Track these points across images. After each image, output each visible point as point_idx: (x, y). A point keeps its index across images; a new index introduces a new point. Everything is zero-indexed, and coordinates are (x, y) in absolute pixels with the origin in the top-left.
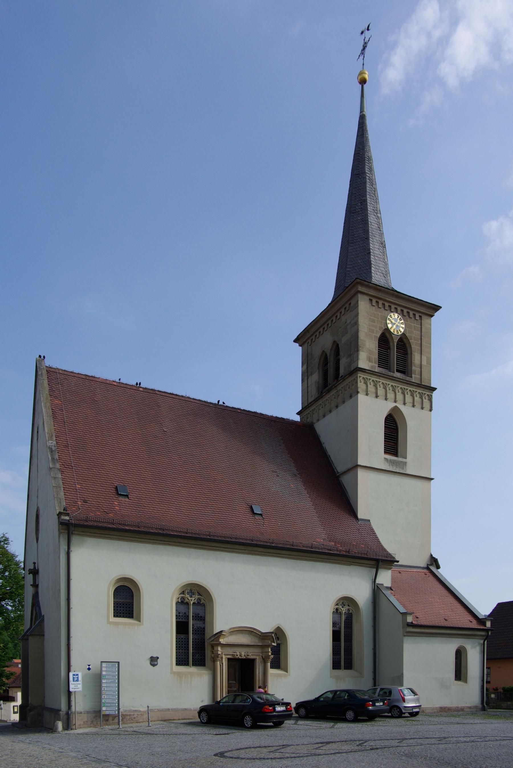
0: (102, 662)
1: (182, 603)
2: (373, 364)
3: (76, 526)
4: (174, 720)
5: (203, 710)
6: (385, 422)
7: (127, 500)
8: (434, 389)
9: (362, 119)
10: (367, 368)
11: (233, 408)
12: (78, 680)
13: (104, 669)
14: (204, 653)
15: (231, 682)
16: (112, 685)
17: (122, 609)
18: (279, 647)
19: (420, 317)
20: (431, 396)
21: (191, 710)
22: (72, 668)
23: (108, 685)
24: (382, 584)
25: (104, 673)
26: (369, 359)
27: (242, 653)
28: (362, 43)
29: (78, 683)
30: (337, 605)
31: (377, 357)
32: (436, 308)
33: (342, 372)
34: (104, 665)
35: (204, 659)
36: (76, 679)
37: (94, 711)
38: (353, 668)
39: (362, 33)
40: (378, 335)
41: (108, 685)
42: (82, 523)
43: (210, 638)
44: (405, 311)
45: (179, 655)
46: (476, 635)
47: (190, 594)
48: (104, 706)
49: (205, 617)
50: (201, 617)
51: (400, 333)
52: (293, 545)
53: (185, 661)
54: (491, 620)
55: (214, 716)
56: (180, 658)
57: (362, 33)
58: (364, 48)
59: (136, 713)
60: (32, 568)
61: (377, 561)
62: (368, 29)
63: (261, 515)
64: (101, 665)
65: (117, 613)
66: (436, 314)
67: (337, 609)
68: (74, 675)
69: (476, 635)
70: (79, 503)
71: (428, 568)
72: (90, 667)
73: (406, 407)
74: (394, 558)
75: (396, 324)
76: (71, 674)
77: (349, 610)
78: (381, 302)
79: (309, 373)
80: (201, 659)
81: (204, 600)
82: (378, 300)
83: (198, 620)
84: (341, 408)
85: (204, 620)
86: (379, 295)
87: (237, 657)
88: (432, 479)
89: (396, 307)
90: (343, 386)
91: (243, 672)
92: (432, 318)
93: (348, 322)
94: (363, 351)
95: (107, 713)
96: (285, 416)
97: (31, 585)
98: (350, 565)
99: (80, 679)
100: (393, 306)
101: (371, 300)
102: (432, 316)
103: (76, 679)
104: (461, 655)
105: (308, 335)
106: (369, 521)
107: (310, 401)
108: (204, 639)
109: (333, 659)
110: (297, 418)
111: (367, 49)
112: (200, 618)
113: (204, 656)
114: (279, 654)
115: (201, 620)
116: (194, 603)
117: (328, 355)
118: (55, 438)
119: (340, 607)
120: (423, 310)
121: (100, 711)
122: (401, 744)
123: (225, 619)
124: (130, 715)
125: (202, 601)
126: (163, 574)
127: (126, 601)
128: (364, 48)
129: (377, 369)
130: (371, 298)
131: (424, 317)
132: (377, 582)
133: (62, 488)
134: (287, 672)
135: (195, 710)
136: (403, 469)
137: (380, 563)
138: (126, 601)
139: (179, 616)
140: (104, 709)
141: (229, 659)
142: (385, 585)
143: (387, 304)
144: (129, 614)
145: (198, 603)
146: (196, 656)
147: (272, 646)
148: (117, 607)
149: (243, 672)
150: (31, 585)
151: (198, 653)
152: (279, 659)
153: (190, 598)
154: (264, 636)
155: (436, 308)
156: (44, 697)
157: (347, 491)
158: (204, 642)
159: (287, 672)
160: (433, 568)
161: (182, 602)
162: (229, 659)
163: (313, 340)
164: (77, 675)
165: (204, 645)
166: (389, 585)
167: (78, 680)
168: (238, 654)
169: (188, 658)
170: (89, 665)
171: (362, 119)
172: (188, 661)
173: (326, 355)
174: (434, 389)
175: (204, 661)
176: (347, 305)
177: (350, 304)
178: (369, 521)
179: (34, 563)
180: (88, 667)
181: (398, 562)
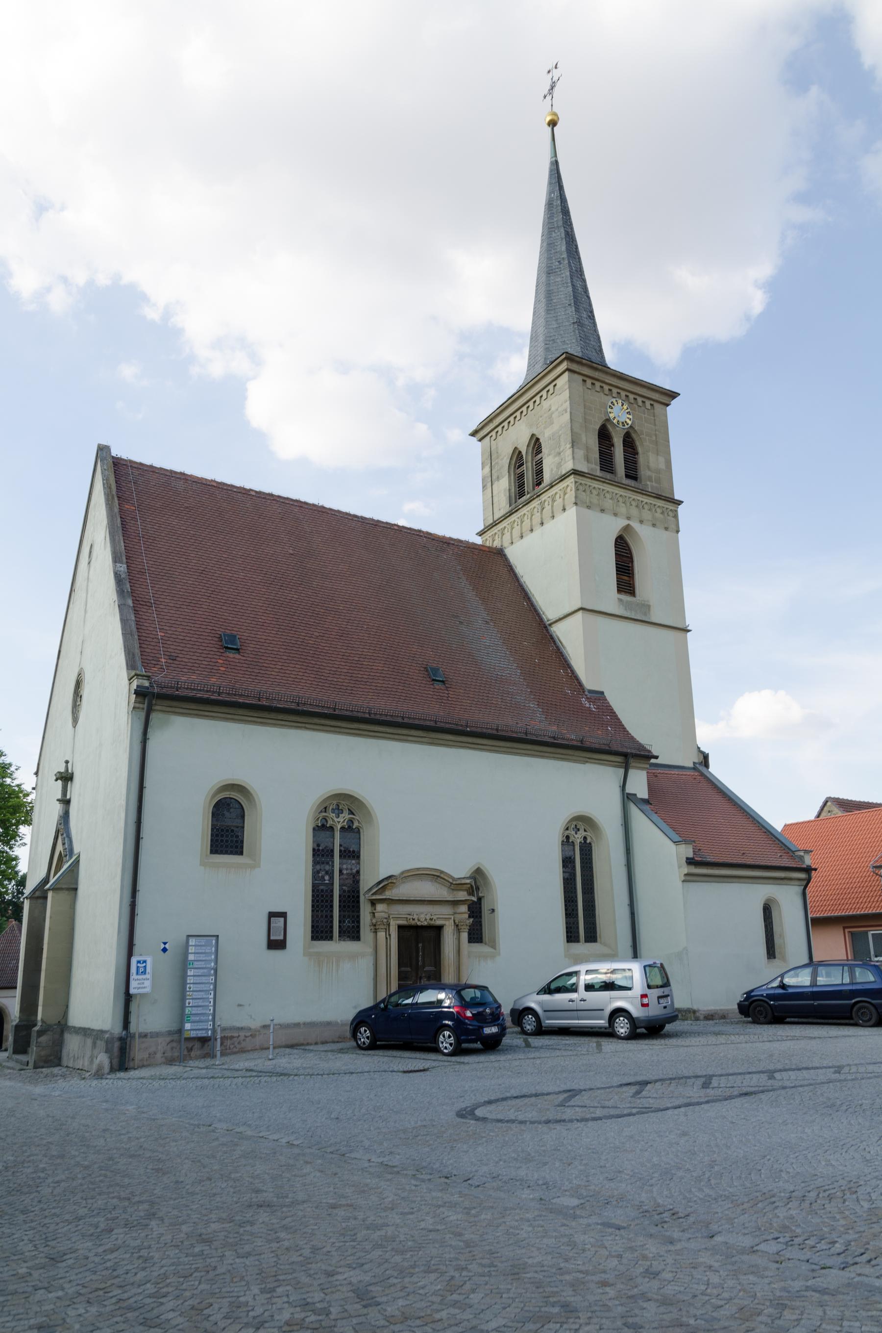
0: (189, 936)
1: (322, 828)
2: (593, 466)
3: (162, 697)
4: (308, 1044)
5: (360, 1020)
6: (616, 544)
7: (237, 656)
8: (679, 503)
9: (555, 166)
10: (586, 471)
11: (387, 523)
12: (144, 973)
13: (191, 950)
14: (359, 917)
15: (403, 969)
16: (204, 980)
17: (224, 838)
18: (480, 904)
19: (652, 405)
20: (676, 511)
21: (336, 1024)
22: (136, 950)
23: (198, 980)
24: (635, 795)
25: (191, 957)
26: (587, 459)
27: (422, 915)
28: (549, 83)
29: (144, 977)
30: (567, 829)
31: (597, 456)
32: (673, 395)
33: (547, 477)
34: (192, 941)
35: (359, 927)
36: (141, 970)
37: (170, 1031)
38: (598, 939)
39: (549, 72)
40: (598, 427)
41: (198, 980)
42: (170, 692)
43: (370, 889)
44: (631, 396)
45: (317, 922)
46: (791, 879)
47: (336, 811)
48: (189, 1021)
49: (359, 852)
50: (354, 851)
51: (627, 426)
52: (497, 730)
53: (326, 932)
54: (36, 1040)
55: (391, 1029)
56: (317, 927)
57: (549, 72)
58: (552, 88)
59: (242, 1034)
60: (63, 770)
61: (625, 755)
62: (556, 68)
63: (443, 681)
64: (187, 942)
65: (217, 846)
66: (672, 402)
67: (568, 837)
68: (139, 962)
69: (791, 879)
70: (163, 660)
71: (695, 769)
72: (167, 946)
73: (643, 526)
74: (649, 751)
75: (620, 414)
76: (134, 961)
77: (585, 838)
78: (598, 384)
79: (494, 477)
80: (353, 927)
81: (359, 822)
82: (594, 382)
83: (349, 857)
84: (549, 525)
85: (358, 857)
86: (596, 374)
87: (413, 923)
88: (689, 631)
89: (619, 391)
90: (550, 495)
91: (419, 951)
92: (668, 408)
93: (553, 409)
94: (578, 448)
95: (193, 1034)
96: (463, 538)
97: (58, 800)
98: (585, 762)
99: (149, 969)
100: (615, 390)
101: (584, 381)
102: (668, 405)
103: (141, 970)
104: (770, 913)
105: (492, 426)
106: (602, 693)
107: (496, 517)
108: (358, 892)
109: (567, 923)
110: (478, 541)
111: (555, 89)
112: (352, 854)
113: (359, 922)
114: (481, 917)
115: (354, 857)
116: (342, 828)
117: (524, 453)
118: (125, 560)
119: (573, 833)
120: (656, 396)
121: (180, 1031)
122: (569, 1113)
123: (387, 854)
124: (232, 1037)
125: (356, 824)
126: (292, 773)
127: (228, 827)
128: (552, 88)
129: (598, 473)
130: (585, 378)
131: (656, 405)
132: (627, 791)
133: (136, 637)
134: (495, 949)
135: (343, 1025)
136: (645, 614)
137: (631, 760)
138: (228, 827)
139: (319, 850)
140: (188, 1026)
141: (400, 927)
142: (639, 796)
143: (606, 387)
144: (237, 847)
145: (349, 827)
146: (344, 922)
147: (469, 903)
148: (217, 835)
149: (419, 951)
150: (58, 800)
151: (349, 917)
152: (481, 925)
153: (336, 820)
154: (455, 885)
155: (673, 395)
156: (67, 1007)
157: (564, 648)
158: (358, 897)
159: (495, 949)
160: (702, 768)
161: (323, 825)
162: (400, 927)
163: (500, 433)
164: (145, 962)
165: (358, 902)
166: (646, 796)
167: (144, 973)
168: (415, 917)
169: (332, 927)
170: (165, 943)
171: (555, 166)
172: (332, 932)
173: (520, 452)
174: (679, 503)
175: (359, 932)
176: (551, 387)
177: (555, 385)
178: (602, 693)
179: (67, 762)
180: (162, 946)
181: (657, 757)
